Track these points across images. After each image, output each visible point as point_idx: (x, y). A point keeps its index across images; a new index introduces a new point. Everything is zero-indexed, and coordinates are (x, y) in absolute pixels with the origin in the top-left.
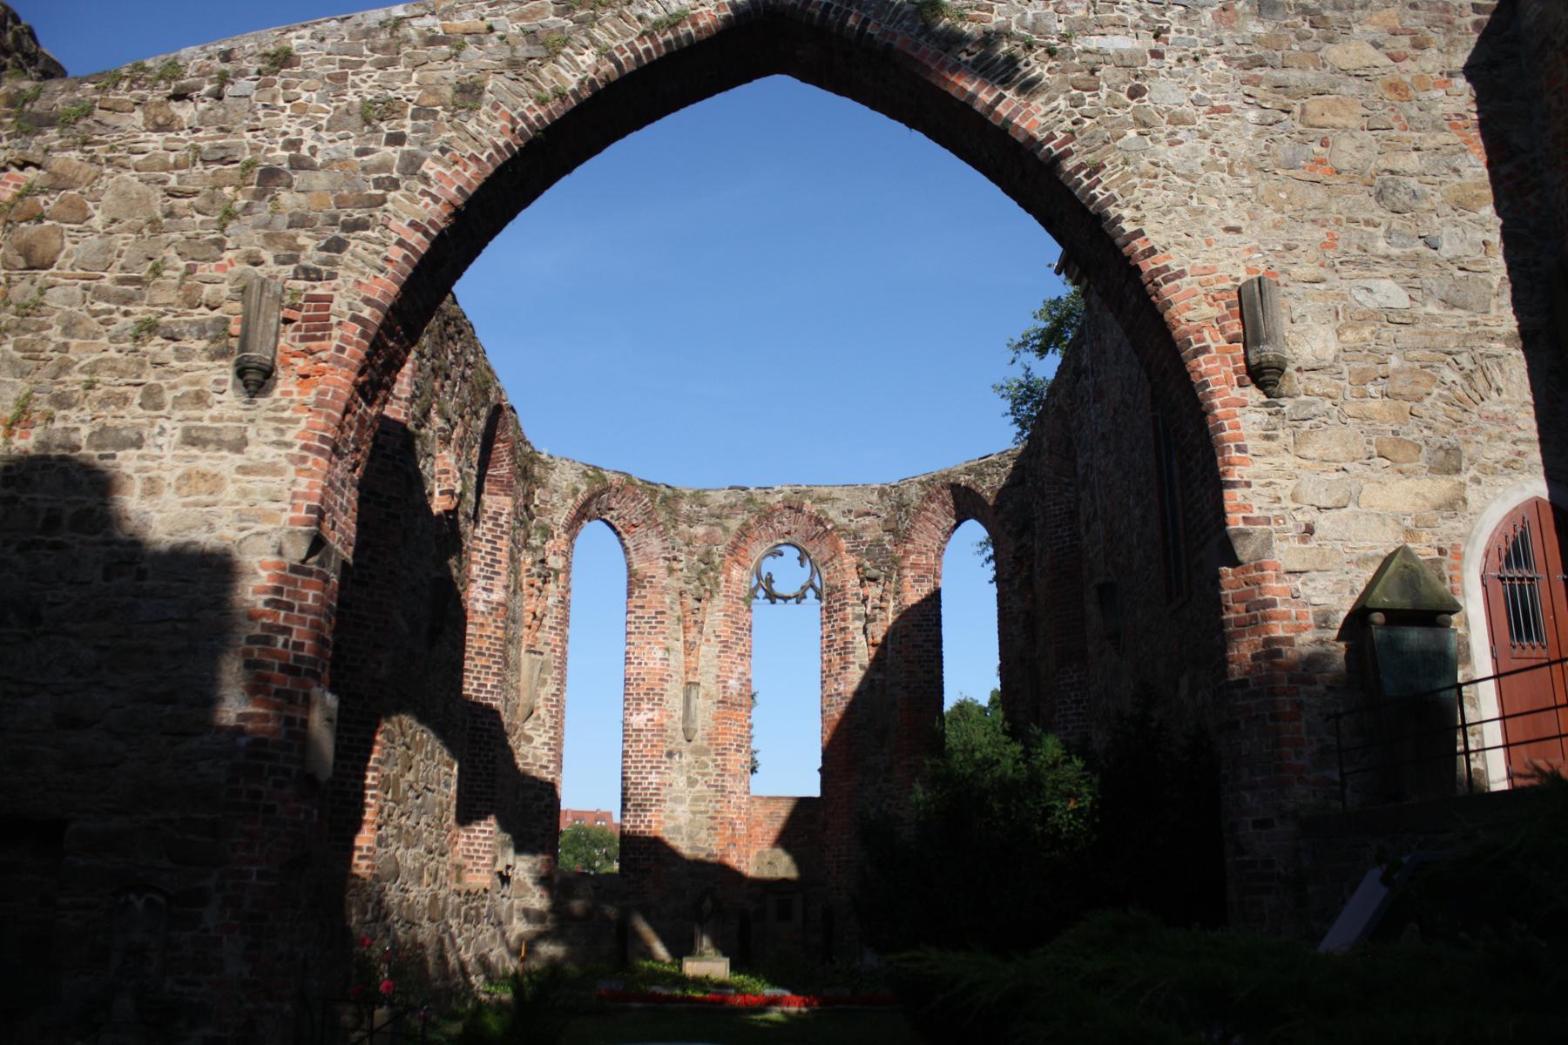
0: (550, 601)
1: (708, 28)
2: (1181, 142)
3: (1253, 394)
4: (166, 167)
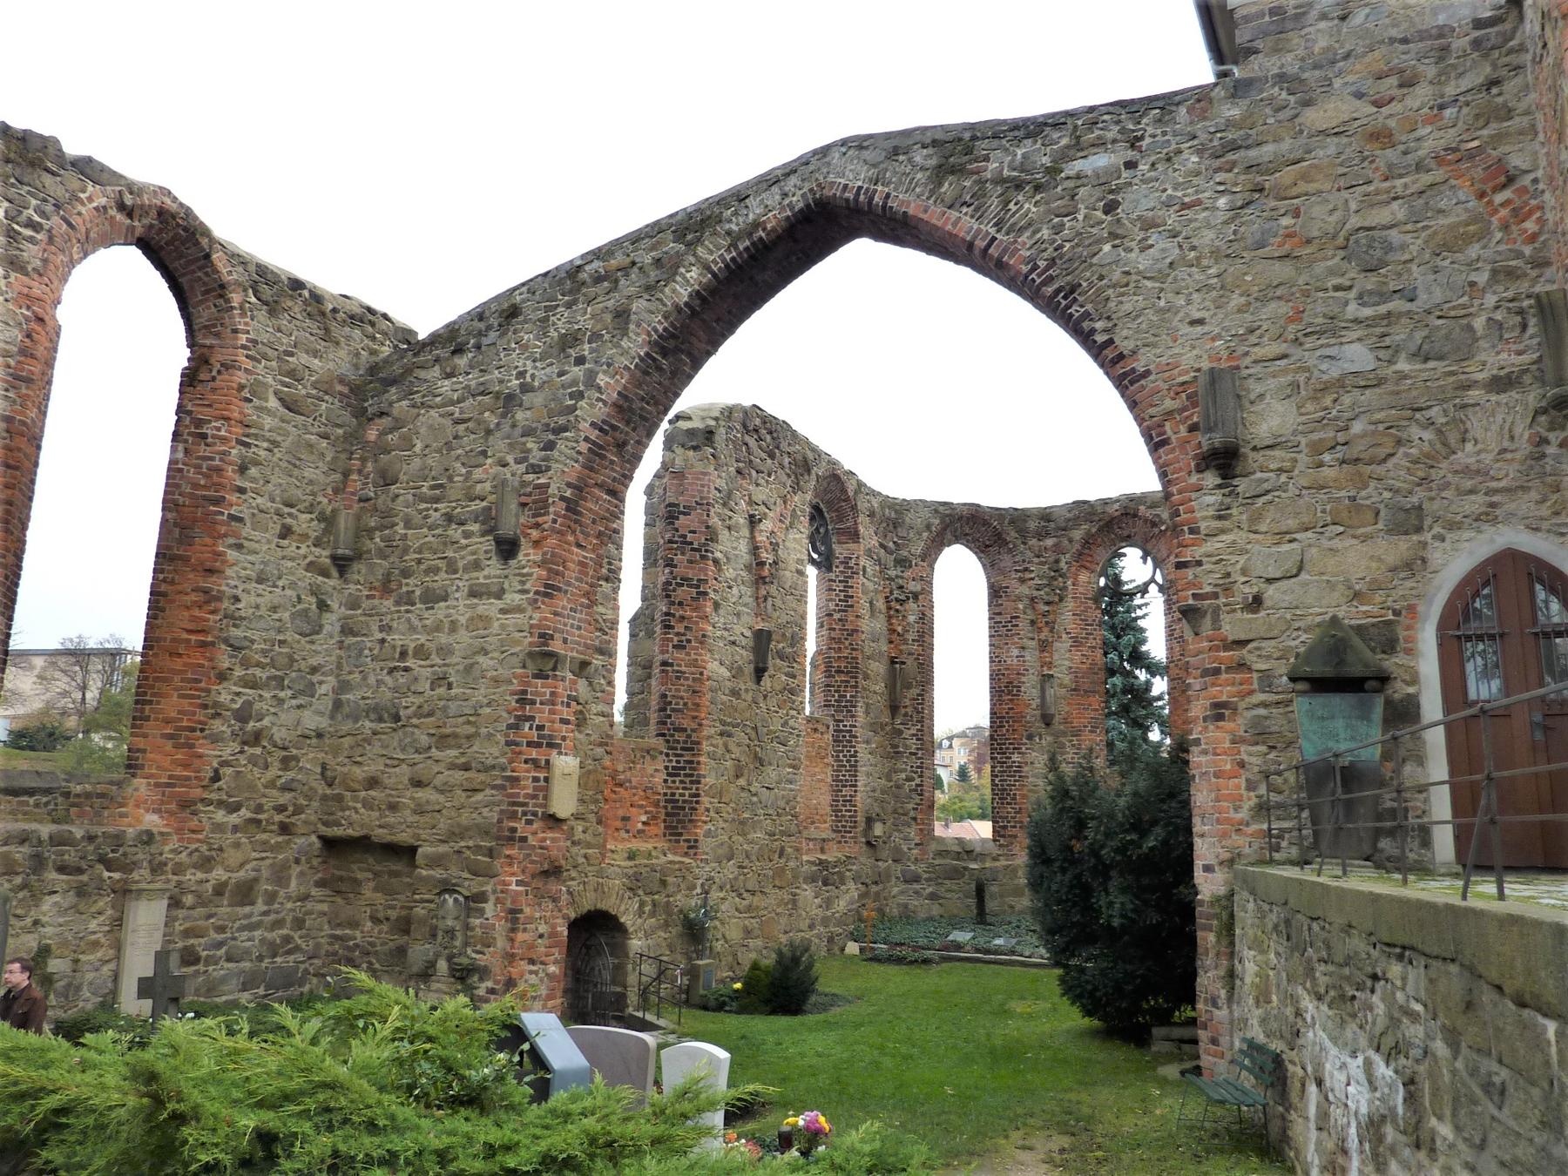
0: (911, 619)
1: (774, 230)
2: (1152, 246)
3: (1211, 479)
4: (453, 403)
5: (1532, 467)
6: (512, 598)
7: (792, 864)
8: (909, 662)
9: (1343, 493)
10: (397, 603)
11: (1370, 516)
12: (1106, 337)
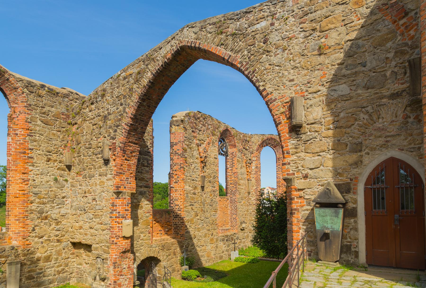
4: (92, 119)
6: (109, 176)
8: (253, 180)
10: (83, 178)
11: (344, 146)
12: (263, 88)
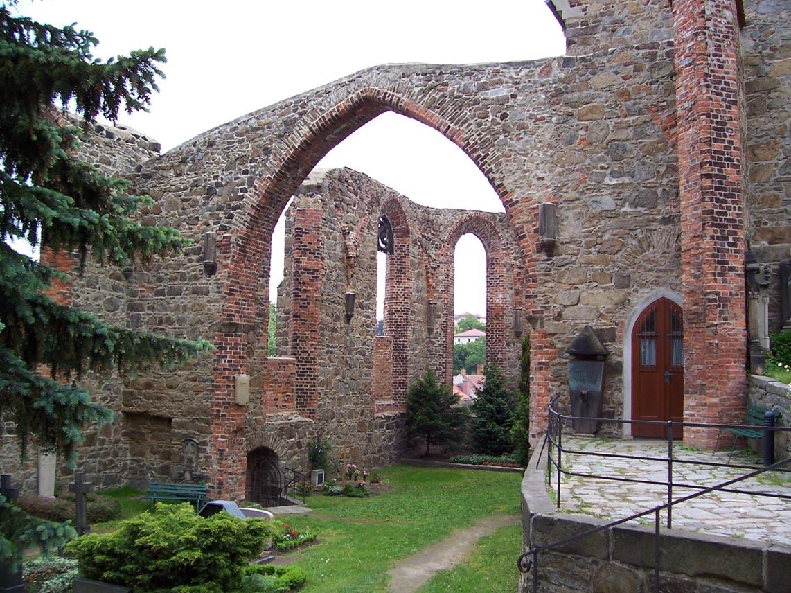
0: (441, 278)
2: (521, 138)
5: (675, 261)
7: (368, 419)
8: (438, 304)
9: (598, 267)
11: (609, 279)
